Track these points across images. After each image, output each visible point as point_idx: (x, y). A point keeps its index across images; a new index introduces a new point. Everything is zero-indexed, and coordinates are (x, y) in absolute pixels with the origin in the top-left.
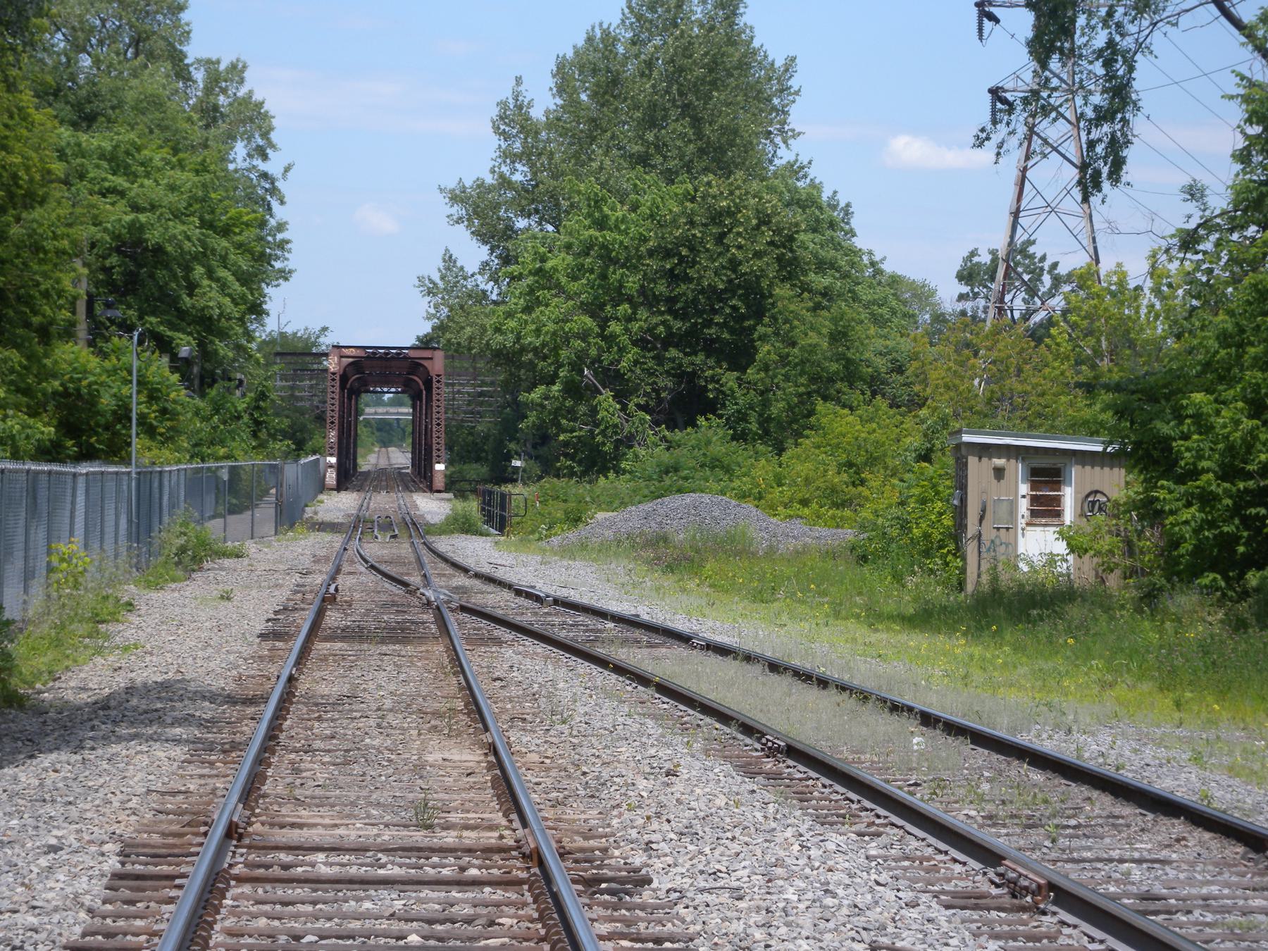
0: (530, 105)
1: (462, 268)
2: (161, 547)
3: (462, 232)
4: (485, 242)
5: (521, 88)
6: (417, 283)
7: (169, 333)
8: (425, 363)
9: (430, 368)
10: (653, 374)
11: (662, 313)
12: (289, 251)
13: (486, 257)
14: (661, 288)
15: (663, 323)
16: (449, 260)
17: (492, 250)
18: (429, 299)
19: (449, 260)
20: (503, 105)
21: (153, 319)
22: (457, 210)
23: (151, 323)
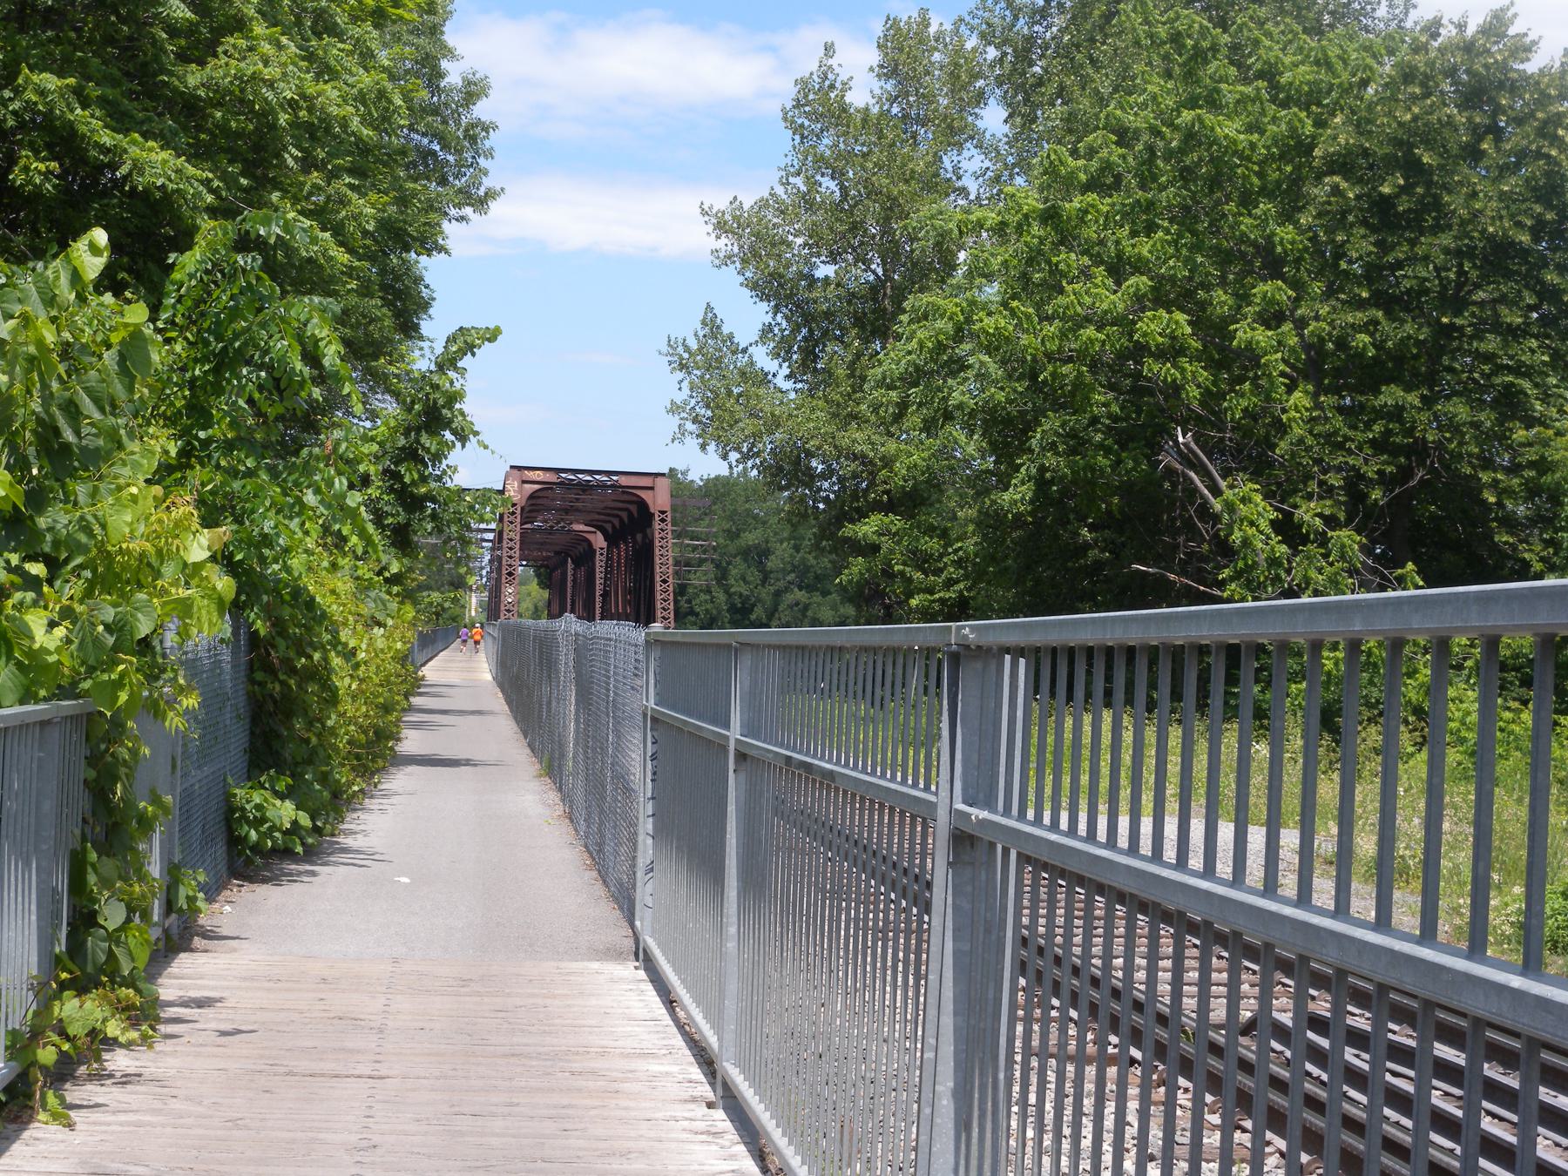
0: (846, 86)
1: (731, 337)
2: (1069, 266)
3: (731, 276)
4: (765, 297)
5: (833, 62)
6: (665, 349)
7: (107, 138)
8: (643, 494)
9: (649, 502)
10: (1340, 446)
11: (1361, 304)
12: (489, 154)
13: (768, 319)
14: (1361, 245)
15: (1366, 327)
16: (712, 324)
17: (776, 310)
18: (680, 375)
19: (712, 324)
20: (804, 84)
21: (50, 81)
22: (724, 244)
23: (42, 93)
